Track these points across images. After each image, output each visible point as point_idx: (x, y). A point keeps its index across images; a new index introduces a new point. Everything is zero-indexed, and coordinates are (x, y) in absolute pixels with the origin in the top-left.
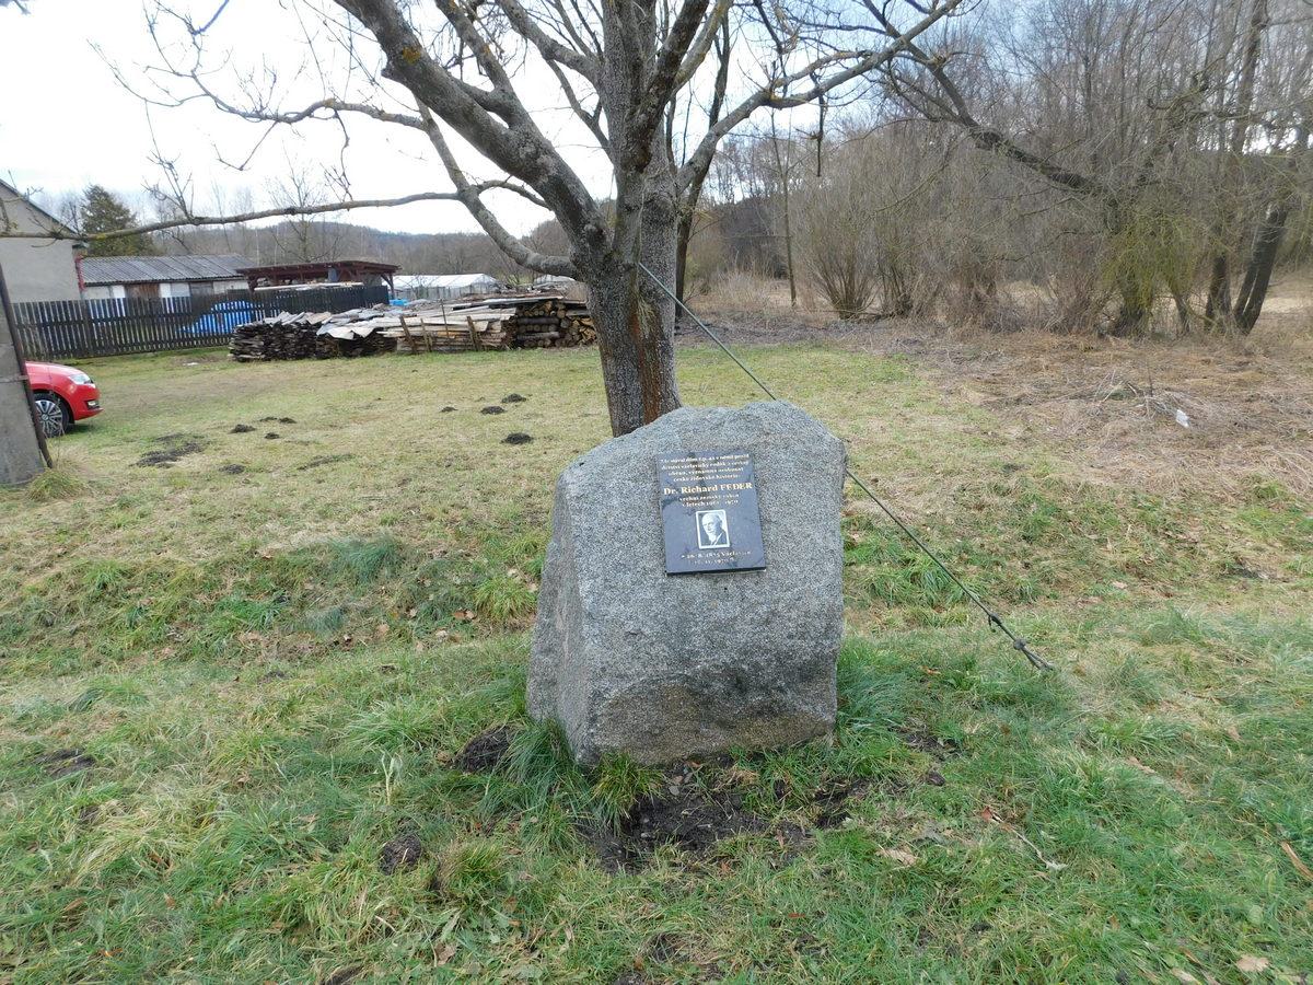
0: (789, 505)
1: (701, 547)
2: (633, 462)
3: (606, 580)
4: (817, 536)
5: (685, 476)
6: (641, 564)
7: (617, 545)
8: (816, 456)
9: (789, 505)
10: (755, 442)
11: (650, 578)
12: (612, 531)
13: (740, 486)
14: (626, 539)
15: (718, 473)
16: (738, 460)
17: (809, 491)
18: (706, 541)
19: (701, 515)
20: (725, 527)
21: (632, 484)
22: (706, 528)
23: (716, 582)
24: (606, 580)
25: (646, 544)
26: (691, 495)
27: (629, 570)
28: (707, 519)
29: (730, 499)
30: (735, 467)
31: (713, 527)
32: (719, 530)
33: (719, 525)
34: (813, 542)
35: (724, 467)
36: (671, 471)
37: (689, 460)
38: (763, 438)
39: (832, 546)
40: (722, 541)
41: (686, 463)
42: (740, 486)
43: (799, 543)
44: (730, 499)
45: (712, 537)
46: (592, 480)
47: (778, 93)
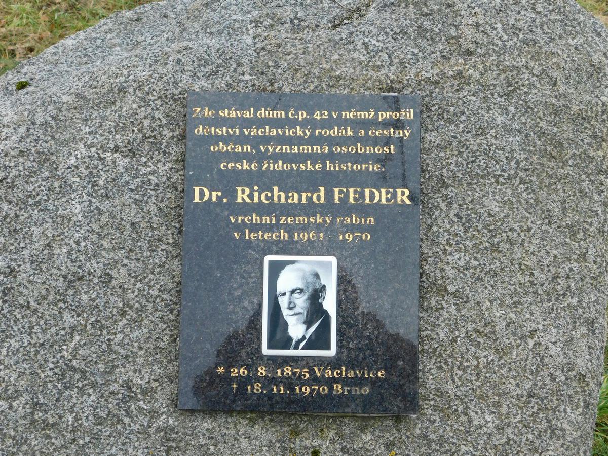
0: (495, 248)
1: (266, 351)
2: (130, 103)
3: (36, 405)
4: (550, 336)
5: (250, 158)
6: (122, 374)
7: (69, 319)
8: (580, 119)
9: (495, 248)
10: (433, 73)
11: (140, 410)
12: (61, 283)
13: (382, 196)
14: (93, 307)
15: (332, 157)
16: (386, 124)
17: (548, 218)
18: (280, 337)
19: (276, 268)
20: (330, 303)
21: (122, 162)
22: (283, 302)
23: (295, 432)
24: (36, 405)
25: (136, 323)
26: (260, 209)
27: (94, 385)
28: (288, 280)
29: (352, 228)
30: (375, 142)
31: (301, 302)
32: (315, 312)
33: (316, 295)
34: (539, 351)
35: (343, 141)
36: (217, 139)
37: (383, 116)
38: (457, 64)
39: (582, 365)
40: (319, 340)
41: (375, 123)
42: (382, 196)
43: (502, 352)
44: (352, 228)
45: (296, 330)
46: (27, 144)
47: (196, 34)
